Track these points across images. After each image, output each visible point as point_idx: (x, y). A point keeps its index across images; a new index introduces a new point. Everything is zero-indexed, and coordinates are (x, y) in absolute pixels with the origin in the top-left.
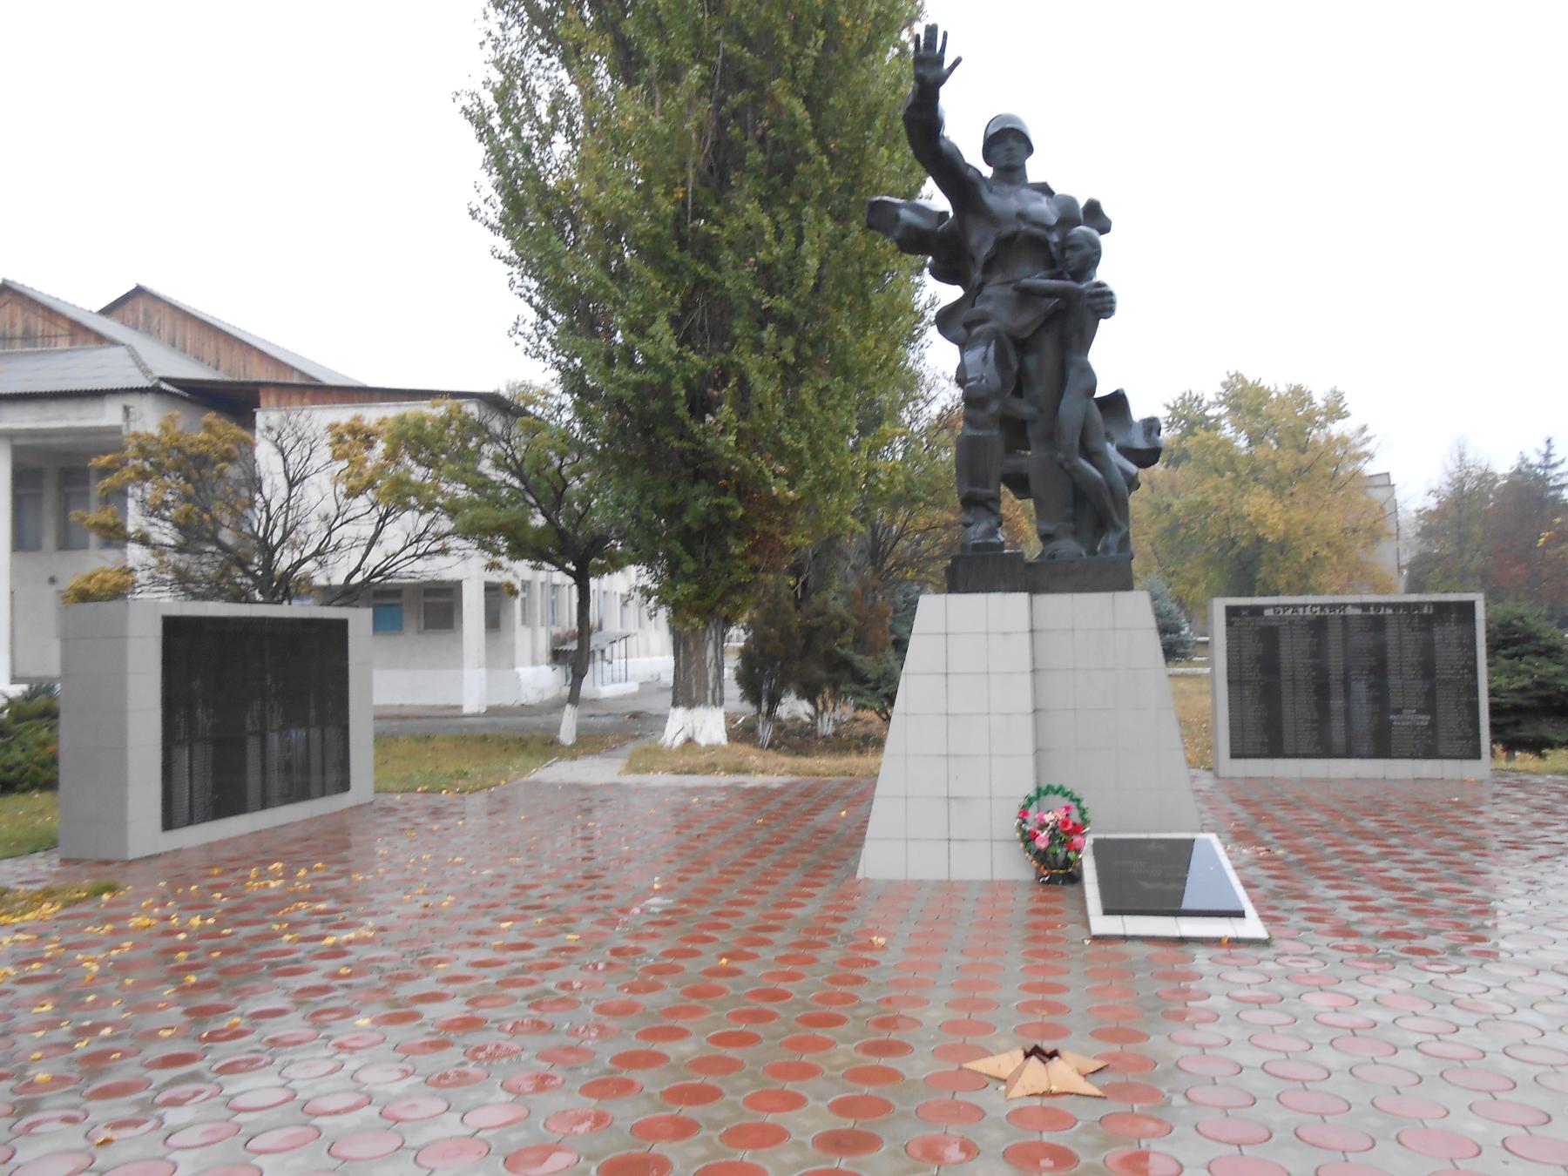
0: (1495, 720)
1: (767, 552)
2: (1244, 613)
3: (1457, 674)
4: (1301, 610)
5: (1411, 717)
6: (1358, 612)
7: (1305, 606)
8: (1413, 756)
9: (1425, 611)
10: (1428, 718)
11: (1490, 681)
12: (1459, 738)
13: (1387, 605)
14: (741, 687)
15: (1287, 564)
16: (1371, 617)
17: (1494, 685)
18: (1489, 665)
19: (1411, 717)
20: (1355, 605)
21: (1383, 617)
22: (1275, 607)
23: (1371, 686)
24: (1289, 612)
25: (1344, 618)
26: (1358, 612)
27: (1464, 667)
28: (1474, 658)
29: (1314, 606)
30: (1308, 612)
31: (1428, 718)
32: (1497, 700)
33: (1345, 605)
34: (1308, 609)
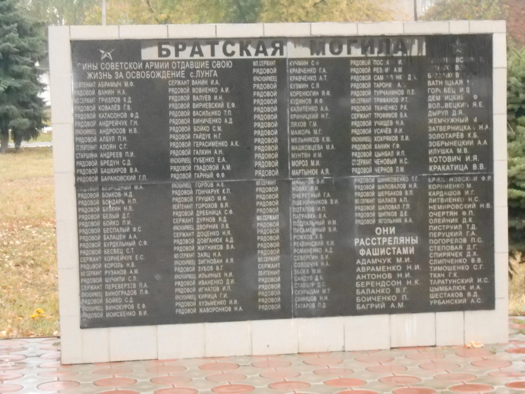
0: (514, 223)
1: (58, 22)
2: (105, 54)
3: (463, 162)
4: (206, 49)
5: (389, 241)
6: (305, 52)
7: (212, 42)
8: (388, 310)
9: (414, 52)
10: (415, 241)
11: (510, 165)
12: (462, 274)
13: (352, 40)
14: (40, 103)
15: (292, 10)
16: (324, 62)
17: (514, 170)
18: (510, 139)
19: (389, 241)
20: (298, 41)
21: (346, 61)
22: (159, 43)
23: (322, 188)
24: (185, 54)
25: (281, 64)
26: (305, 52)
27: (473, 150)
28: (488, 135)
29: (230, 41)
30: (219, 54)
31: (415, 241)
32: (517, 193)
33: (282, 41)
34: (219, 48)
